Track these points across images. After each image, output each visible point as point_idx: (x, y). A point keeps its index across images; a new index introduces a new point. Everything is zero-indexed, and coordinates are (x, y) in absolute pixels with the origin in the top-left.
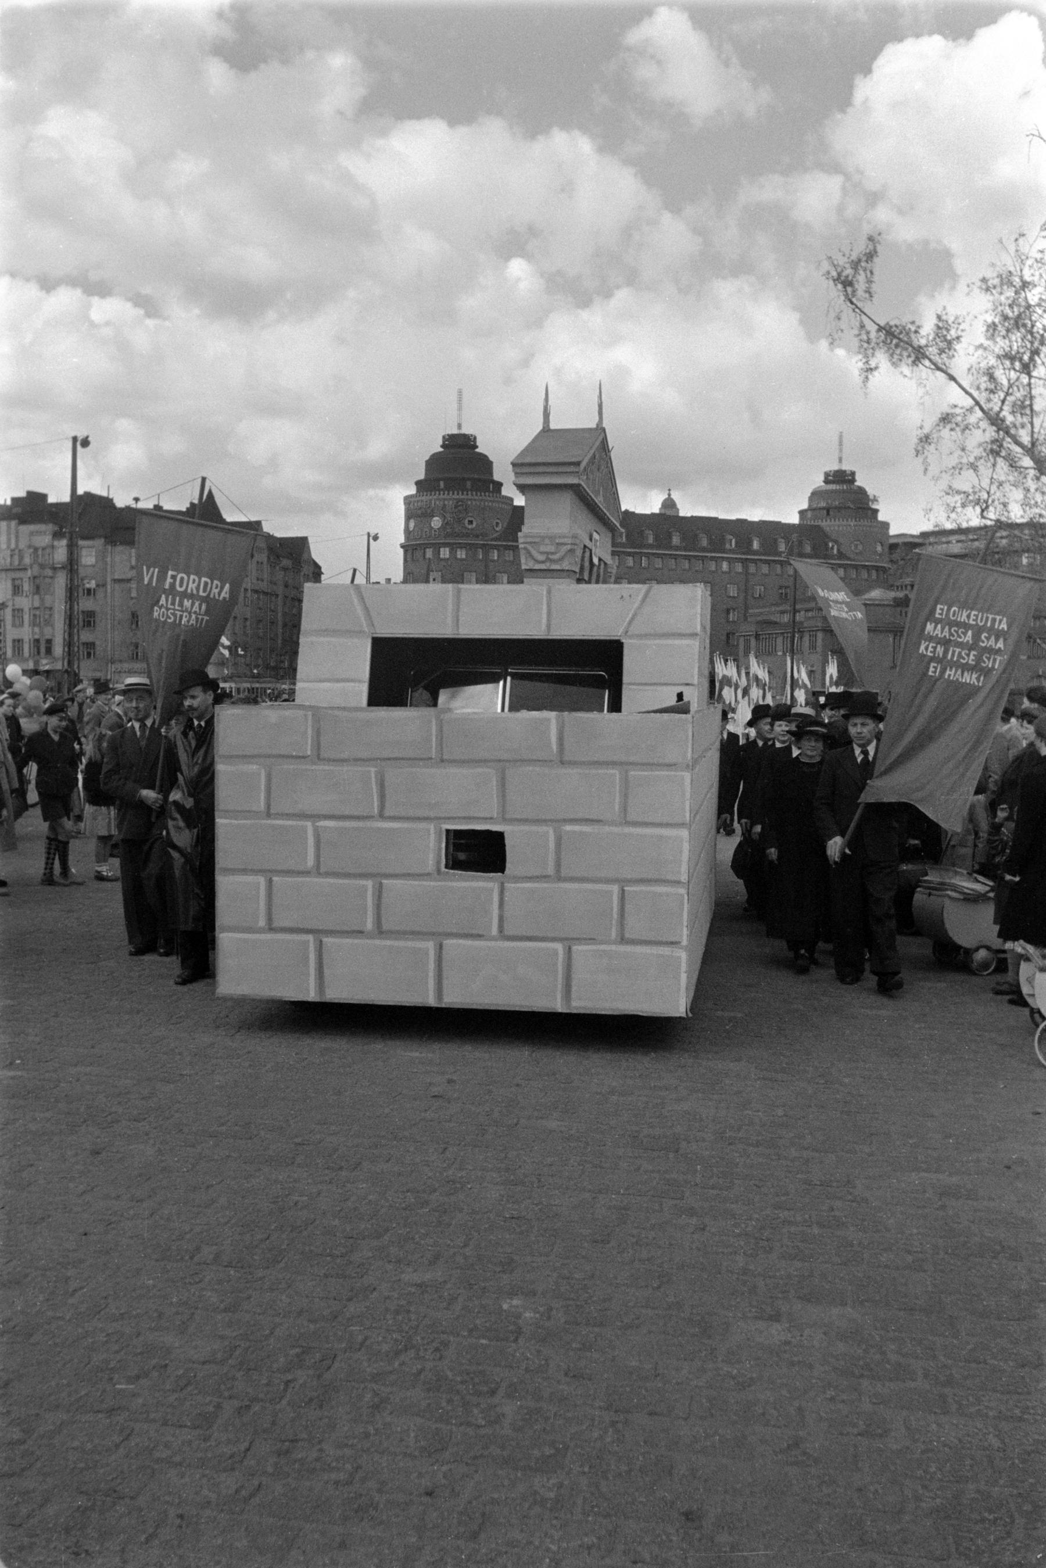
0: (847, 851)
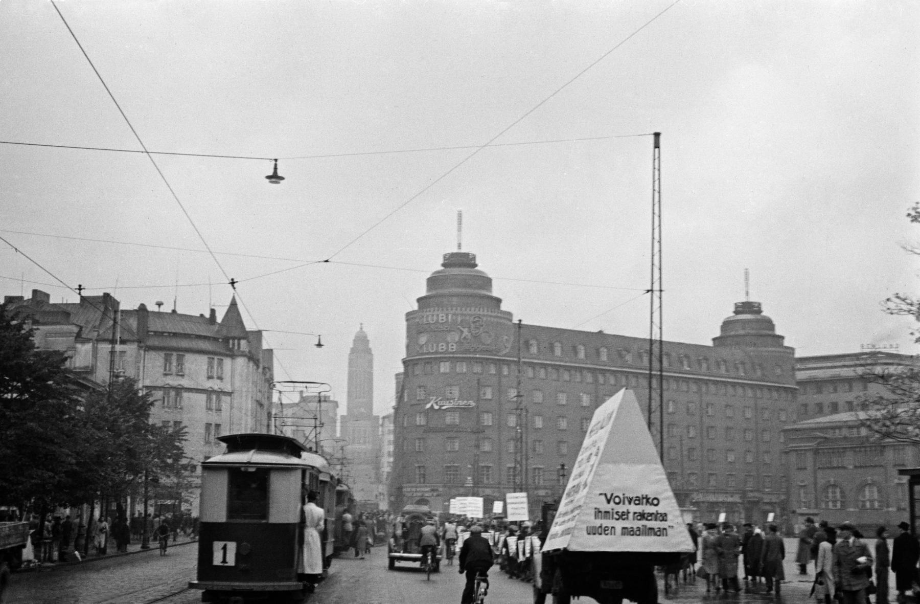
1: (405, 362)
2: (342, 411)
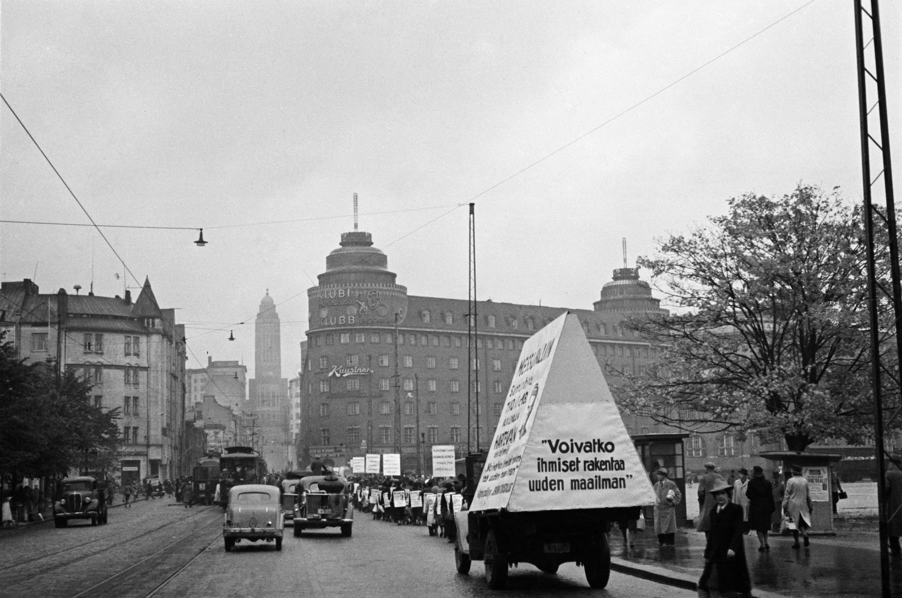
0: (382, 518)
1: (308, 334)
2: (251, 375)
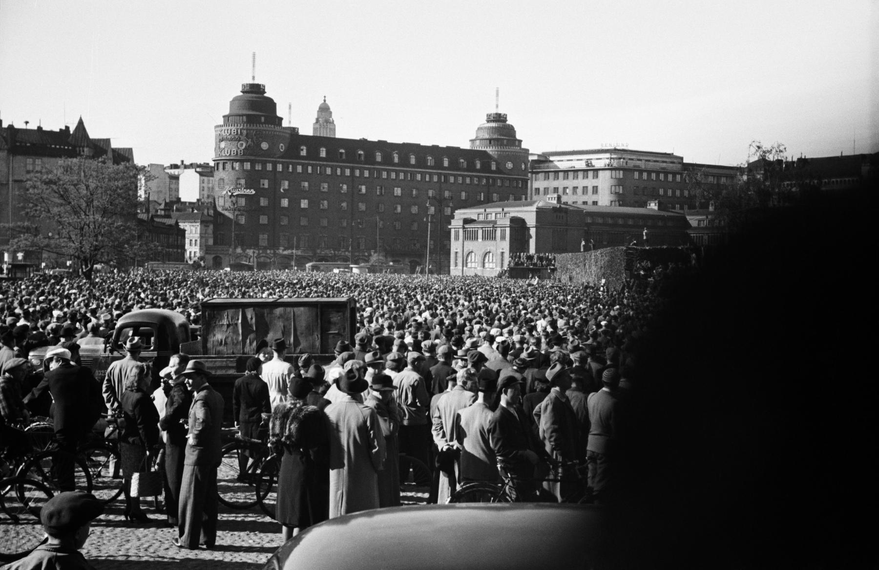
0: (530, 276)
